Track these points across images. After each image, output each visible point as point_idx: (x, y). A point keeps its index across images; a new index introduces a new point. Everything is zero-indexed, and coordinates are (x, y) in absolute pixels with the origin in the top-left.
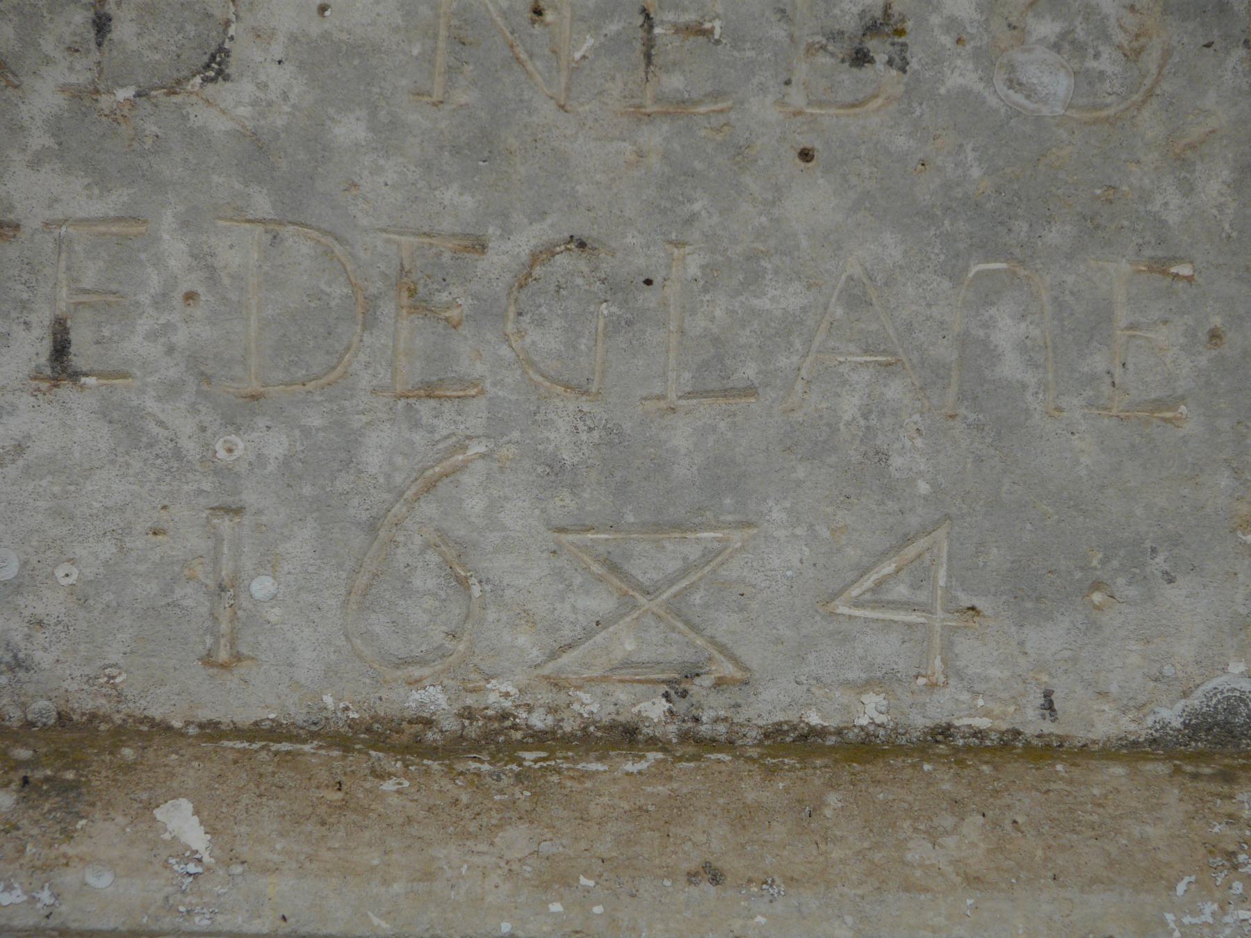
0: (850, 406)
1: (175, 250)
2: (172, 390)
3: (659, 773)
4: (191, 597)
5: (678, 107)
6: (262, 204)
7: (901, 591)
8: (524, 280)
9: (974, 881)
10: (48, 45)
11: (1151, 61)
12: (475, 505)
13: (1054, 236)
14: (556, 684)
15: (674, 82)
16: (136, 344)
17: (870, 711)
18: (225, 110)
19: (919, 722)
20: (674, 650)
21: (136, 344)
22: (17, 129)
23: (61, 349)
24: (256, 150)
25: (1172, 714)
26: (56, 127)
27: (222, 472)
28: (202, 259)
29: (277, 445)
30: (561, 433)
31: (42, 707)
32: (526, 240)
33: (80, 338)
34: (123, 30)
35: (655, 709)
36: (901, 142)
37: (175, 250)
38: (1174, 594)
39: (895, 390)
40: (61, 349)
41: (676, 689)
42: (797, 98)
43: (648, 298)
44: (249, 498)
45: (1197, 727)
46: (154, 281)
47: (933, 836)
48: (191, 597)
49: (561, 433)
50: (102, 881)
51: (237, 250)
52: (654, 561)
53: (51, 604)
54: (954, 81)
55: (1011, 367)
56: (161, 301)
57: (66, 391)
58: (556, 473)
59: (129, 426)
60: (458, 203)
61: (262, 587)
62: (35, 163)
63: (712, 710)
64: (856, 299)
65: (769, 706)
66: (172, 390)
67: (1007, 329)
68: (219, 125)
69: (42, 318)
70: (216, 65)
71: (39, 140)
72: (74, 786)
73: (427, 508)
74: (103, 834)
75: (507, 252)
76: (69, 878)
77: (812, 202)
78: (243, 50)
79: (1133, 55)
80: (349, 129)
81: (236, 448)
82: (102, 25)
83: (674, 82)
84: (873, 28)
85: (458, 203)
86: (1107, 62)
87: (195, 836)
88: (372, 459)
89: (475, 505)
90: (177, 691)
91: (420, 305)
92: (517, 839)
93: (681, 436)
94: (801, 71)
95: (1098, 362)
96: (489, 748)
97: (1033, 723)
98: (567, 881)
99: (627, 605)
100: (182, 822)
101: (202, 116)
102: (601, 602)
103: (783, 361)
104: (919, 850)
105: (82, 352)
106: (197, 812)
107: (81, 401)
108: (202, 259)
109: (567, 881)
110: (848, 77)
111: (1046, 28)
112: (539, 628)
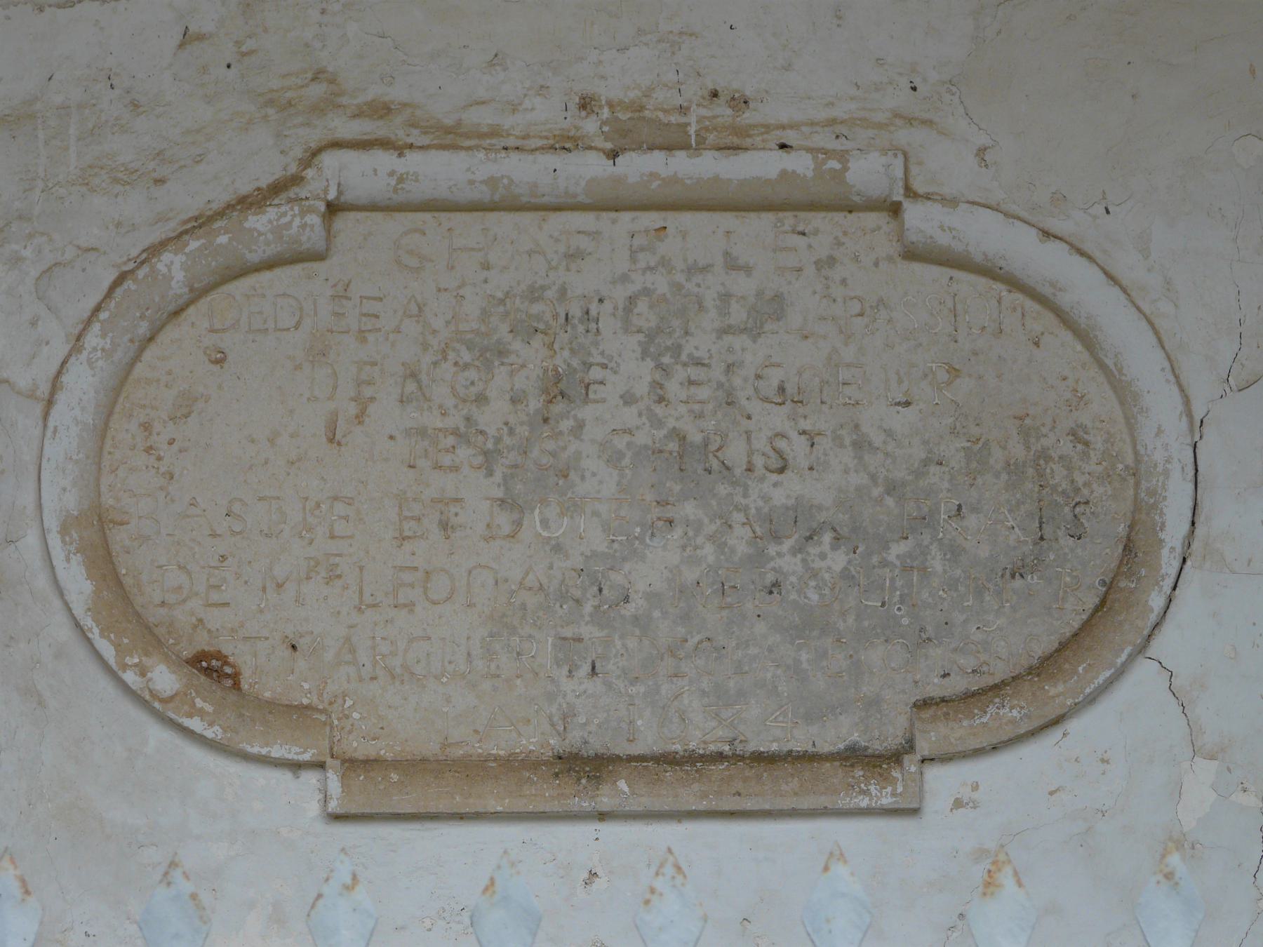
0: (769, 675)
1: (618, 643)
2: (619, 677)
3: (727, 768)
4: (624, 725)
5: (729, 606)
6: (637, 632)
7: (781, 719)
8: (696, 648)
9: (796, 794)
10: (588, 596)
11: (837, 590)
12: (686, 702)
13: (815, 633)
14: (705, 742)
15: (729, 600)
16: (610, 667)
17: (774, 747)
18: (629, 610)
19: (785, 749)
20: (729, 734)
21: (610, 667)
22: (583, 616)
23: (593, 668)
24: (636, 619)
25: (842, 746)
26: (591, 615)
27: (630, 696)
28: (624, 645)
29: (642, 689)
30: (705, 684)
31: (592, 753)
32: (697, 639)
33: (598, 665)
34: (605, 592)
35: (727, 748)
36: (780, 613)
37: (618, 643)
38: (842, 718)
39: (779, 672)
40: (593, 668)
41: (731, 743)
42: (757, 602)
43: (724, 652)
44: (636, 702)
45: (847, 749)
46: (614, 651)
47: (787, 783)
48: (624, 725)
49: (705, 684)
50: (605, 800)
51: (632, 643)
52: (725, 714)
53: (593, 728)
54: (792, 597)
55: (805, 665)
56: (616, 656)
57: (595, 678)
58: (704, 693)
59: (609, 686)
60: (681, 630)
61: (639, 723)
62: (587, 624)
63: (739, 748)
64: (770, 650)
65: (752, 747)
66: (619, 677)
67: (804, 656)
68: (628, 614)
69: (589, 661)
70: (626, 599)
71: (587, 618)
72: (597, 777)
73: (676, 703)
74: (605, 789)
75: (693, 641)
76: (598, 799)
77: (760, 628)
78: (632, 596)
79: (832, 589)
80: (656, 614)
81: (633, 690)
82: (600, 590)
83: (729, 600)
84: (774, 585)
85: (681, 630)
86: (827, 591)
87: (626, 789)
88: (663, 692)
89: (686, 702)
90: (623, 749)
91: (673, 655)
92: (696, 787)
93: (732, 684)
94: (758, 596)
95: (825, 663)
96: (691, 759)
97: (811, 749)
98: (707, 796)
99: (720, 723)
100: (622, 785)
101: (623, 612)
102: (714, 724)
103: (754, 666)
104: (784, 787)
105: (598, 669)
106: (794, 172)
107: (598, 680)
108: (624, 645)
109: (707, 796)
110: (768, 597)
111: (813, 583)
112: (702, 733)
